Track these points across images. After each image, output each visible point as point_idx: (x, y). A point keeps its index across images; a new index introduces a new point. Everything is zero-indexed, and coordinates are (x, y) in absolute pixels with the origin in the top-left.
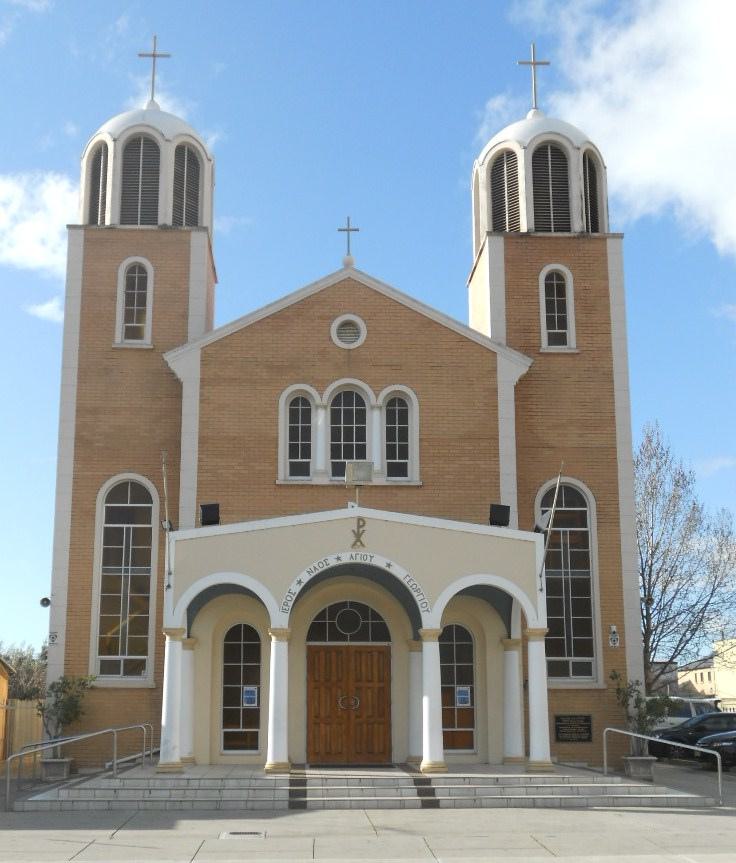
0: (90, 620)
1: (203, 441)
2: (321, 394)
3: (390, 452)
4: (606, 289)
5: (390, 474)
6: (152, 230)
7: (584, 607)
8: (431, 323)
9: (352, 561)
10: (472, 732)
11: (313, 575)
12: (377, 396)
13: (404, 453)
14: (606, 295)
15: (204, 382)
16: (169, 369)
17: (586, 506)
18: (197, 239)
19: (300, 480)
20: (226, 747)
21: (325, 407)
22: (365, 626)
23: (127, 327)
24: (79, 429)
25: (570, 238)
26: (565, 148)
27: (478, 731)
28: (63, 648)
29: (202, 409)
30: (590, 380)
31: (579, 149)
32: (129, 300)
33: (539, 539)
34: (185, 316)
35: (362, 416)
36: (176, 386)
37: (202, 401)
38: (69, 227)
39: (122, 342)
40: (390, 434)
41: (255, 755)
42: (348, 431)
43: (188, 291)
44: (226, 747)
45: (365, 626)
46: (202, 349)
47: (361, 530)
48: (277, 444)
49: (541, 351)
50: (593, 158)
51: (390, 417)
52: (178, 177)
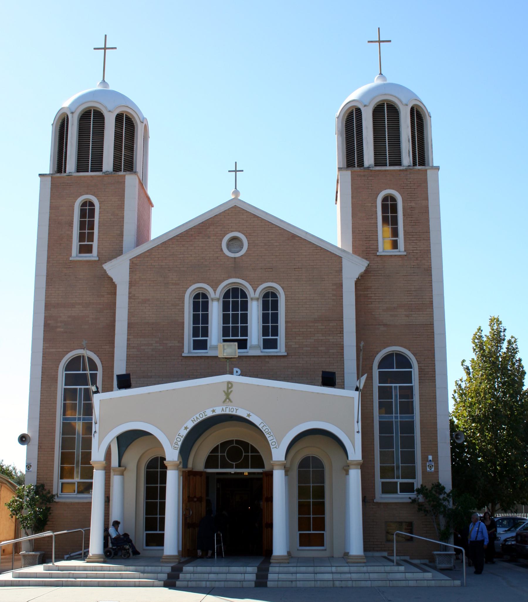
0: (54, 454)
1: (130, 326)
2: (215, 291)
3: (265, 331)
4: (427, 207)
5: (265, 347)
6: (99, 176)
7: (408, 442)
8: (294, 236)
9: (223, 413)
10: (323, 534)
11: (196, 423)
12: (255, 291)
13: (275, 332)
14: (427, 212)
15: (132, 284)
16: (107, 275)
17: (411, 368)
18: (130, 180)
19: (200, 353)
20: (301, 545)
21: (218, 300)
22: (247, 457)
23: (80, 245)
24: (46, 318)
25: (400, 170)
26: (395, 104)
27: (327, 534)
28: (35, 475)
29: (130, 303)
30: (415, 274)
31: (407, 105)
32: (82, 225)
33: (356, 395)
34: (121, 235)
35: (245, 306)
36: (113, 287)
37: (130, 298)
38: (40, 175)
39: (77, 256)
40: (265, 318)
41: (322, 550)
42: (235, 316)
43: (123, 218)
44: (301, 545)
45: (247, 457)
46: (130, 260)
47: (230, 390)
48: (183, 327)
49: (378, 254)
50: (420, 110)
51: (265, 306)
52: (118, 137)
